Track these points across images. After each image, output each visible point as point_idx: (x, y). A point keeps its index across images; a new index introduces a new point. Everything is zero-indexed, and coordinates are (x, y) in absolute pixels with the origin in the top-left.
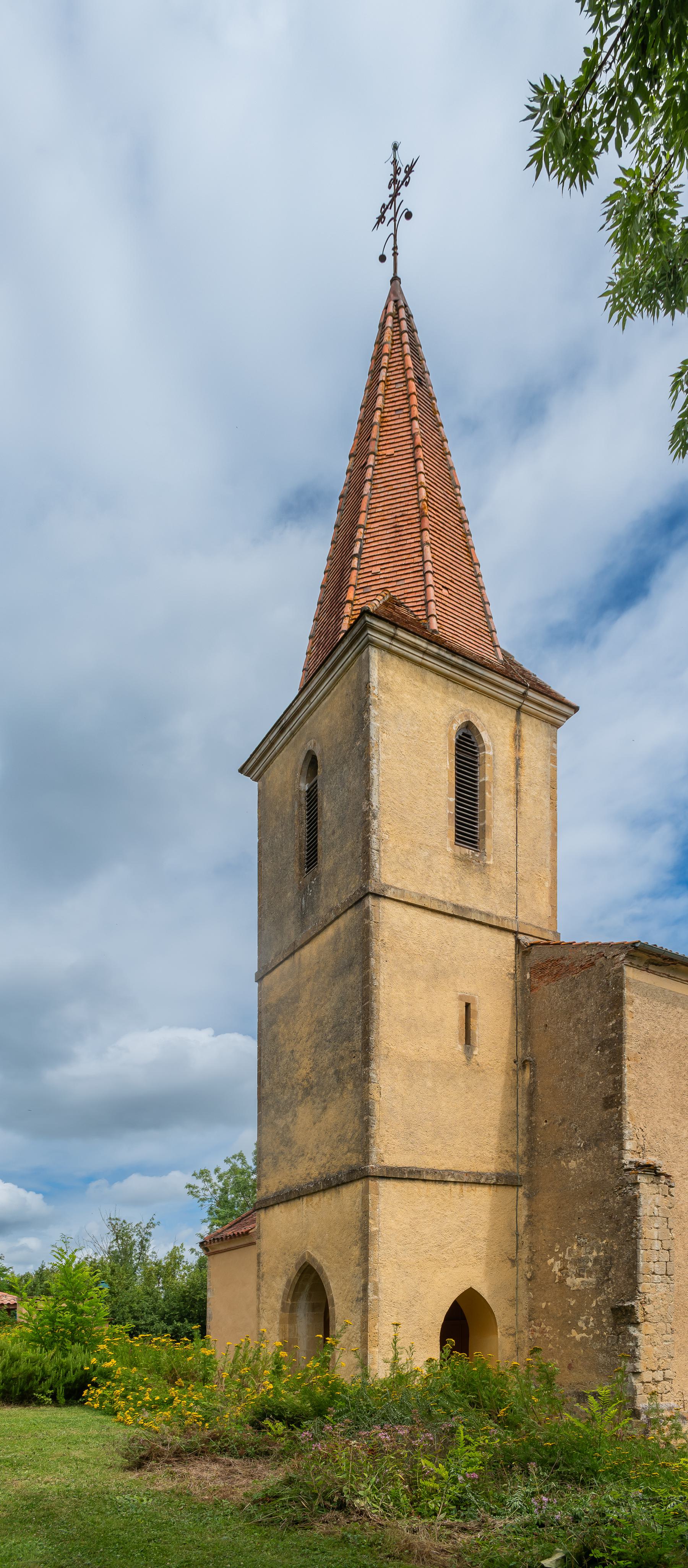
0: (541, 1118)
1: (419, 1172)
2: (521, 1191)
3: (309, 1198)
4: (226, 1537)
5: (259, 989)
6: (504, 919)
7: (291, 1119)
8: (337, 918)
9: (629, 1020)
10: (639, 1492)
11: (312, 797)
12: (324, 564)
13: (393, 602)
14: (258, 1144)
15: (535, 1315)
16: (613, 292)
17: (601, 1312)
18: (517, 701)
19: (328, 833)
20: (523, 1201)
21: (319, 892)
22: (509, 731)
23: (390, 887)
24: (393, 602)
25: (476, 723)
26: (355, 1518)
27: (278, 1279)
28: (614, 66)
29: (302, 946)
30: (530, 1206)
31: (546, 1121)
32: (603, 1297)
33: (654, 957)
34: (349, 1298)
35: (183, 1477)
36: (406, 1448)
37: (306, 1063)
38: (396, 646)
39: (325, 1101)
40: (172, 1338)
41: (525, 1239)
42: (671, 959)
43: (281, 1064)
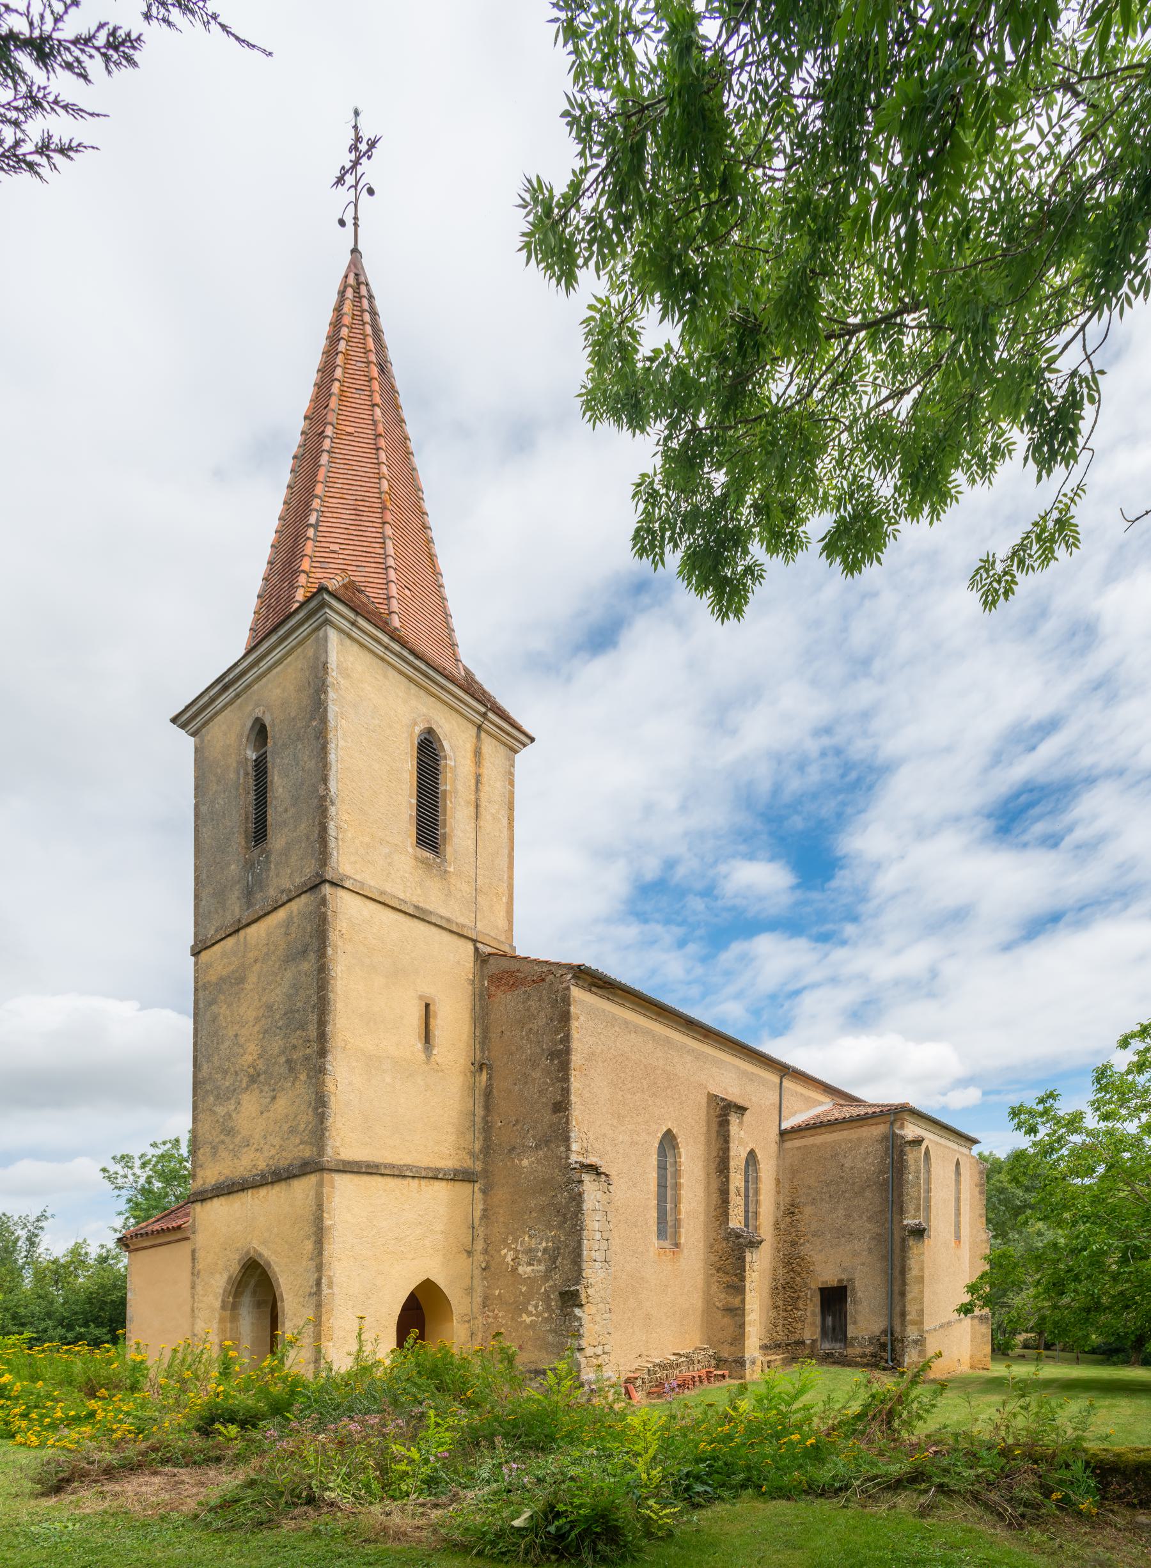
0: (497, 1118)
1: (377, 1166)
2: (477, 1186)
3: (255, 1191)
4: (180, 1550)
5: (196, 964)
6: (464, 926)
8: (290, 900)
9: (575, 1035)
10: (592, 1450)
11: (261, 769)
12: (275, 524)
13: (351, 586)
14: (194, 1133)
15: (489, 1302)
16: (587, 394)
18: (478, 719)
19: (280, 810)
20: (479, 1196)
21: (269, 869)
22: (469, 746)
23: (348, 878)
24: (351, 586)
25: (438, 731)
26: (325, 1510)
27: (218, 1276)
28: (595, 197)
29: (248, 925)
30: (485, 1201)
32: (551, 1283)
34: (300, 1293)
35: (116, 1495)
36: (377, 1436)
37: (253, 1049)
38: (356, 633)
40: (88, 1345)
41: (480, 1231)
43: (222, 1047)
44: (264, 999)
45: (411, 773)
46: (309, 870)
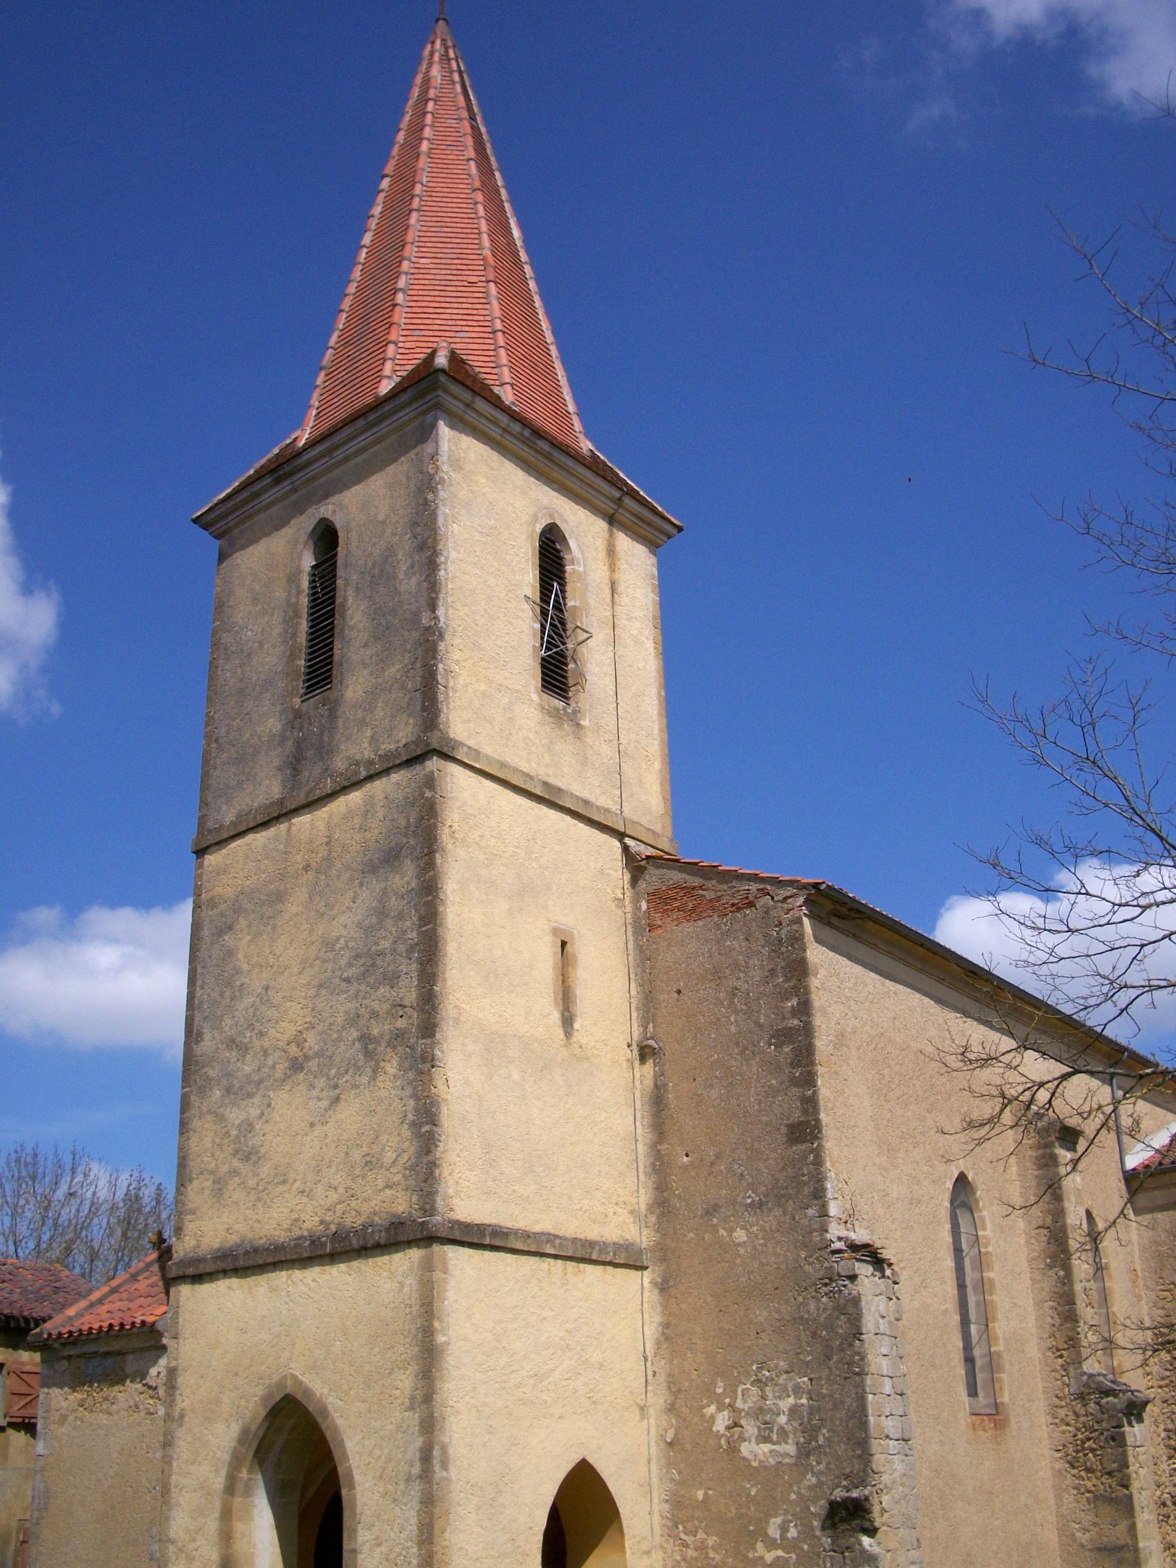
6: (607, 810)
7: (258, 1112)
17: (808, 1508)
22: (601, 544)
25: (562, 526)
31: (687, 1155)
33: (838, 907)
39: (336, 1087)
42: (859, 912)
44: (321, 930)
45: (533, 587)
46: (404, 732)
